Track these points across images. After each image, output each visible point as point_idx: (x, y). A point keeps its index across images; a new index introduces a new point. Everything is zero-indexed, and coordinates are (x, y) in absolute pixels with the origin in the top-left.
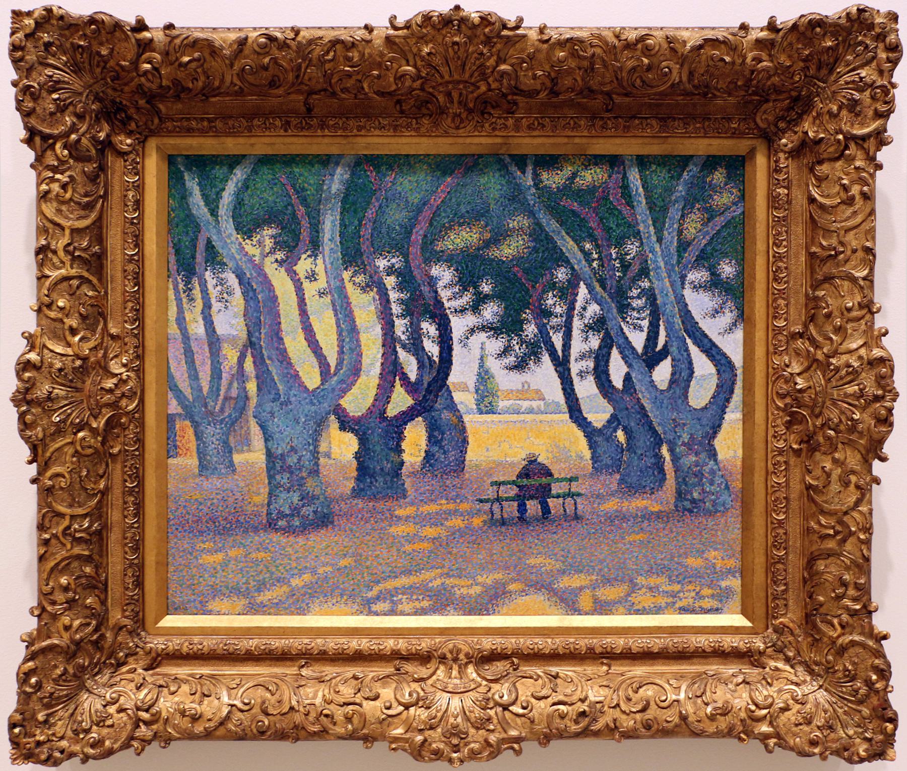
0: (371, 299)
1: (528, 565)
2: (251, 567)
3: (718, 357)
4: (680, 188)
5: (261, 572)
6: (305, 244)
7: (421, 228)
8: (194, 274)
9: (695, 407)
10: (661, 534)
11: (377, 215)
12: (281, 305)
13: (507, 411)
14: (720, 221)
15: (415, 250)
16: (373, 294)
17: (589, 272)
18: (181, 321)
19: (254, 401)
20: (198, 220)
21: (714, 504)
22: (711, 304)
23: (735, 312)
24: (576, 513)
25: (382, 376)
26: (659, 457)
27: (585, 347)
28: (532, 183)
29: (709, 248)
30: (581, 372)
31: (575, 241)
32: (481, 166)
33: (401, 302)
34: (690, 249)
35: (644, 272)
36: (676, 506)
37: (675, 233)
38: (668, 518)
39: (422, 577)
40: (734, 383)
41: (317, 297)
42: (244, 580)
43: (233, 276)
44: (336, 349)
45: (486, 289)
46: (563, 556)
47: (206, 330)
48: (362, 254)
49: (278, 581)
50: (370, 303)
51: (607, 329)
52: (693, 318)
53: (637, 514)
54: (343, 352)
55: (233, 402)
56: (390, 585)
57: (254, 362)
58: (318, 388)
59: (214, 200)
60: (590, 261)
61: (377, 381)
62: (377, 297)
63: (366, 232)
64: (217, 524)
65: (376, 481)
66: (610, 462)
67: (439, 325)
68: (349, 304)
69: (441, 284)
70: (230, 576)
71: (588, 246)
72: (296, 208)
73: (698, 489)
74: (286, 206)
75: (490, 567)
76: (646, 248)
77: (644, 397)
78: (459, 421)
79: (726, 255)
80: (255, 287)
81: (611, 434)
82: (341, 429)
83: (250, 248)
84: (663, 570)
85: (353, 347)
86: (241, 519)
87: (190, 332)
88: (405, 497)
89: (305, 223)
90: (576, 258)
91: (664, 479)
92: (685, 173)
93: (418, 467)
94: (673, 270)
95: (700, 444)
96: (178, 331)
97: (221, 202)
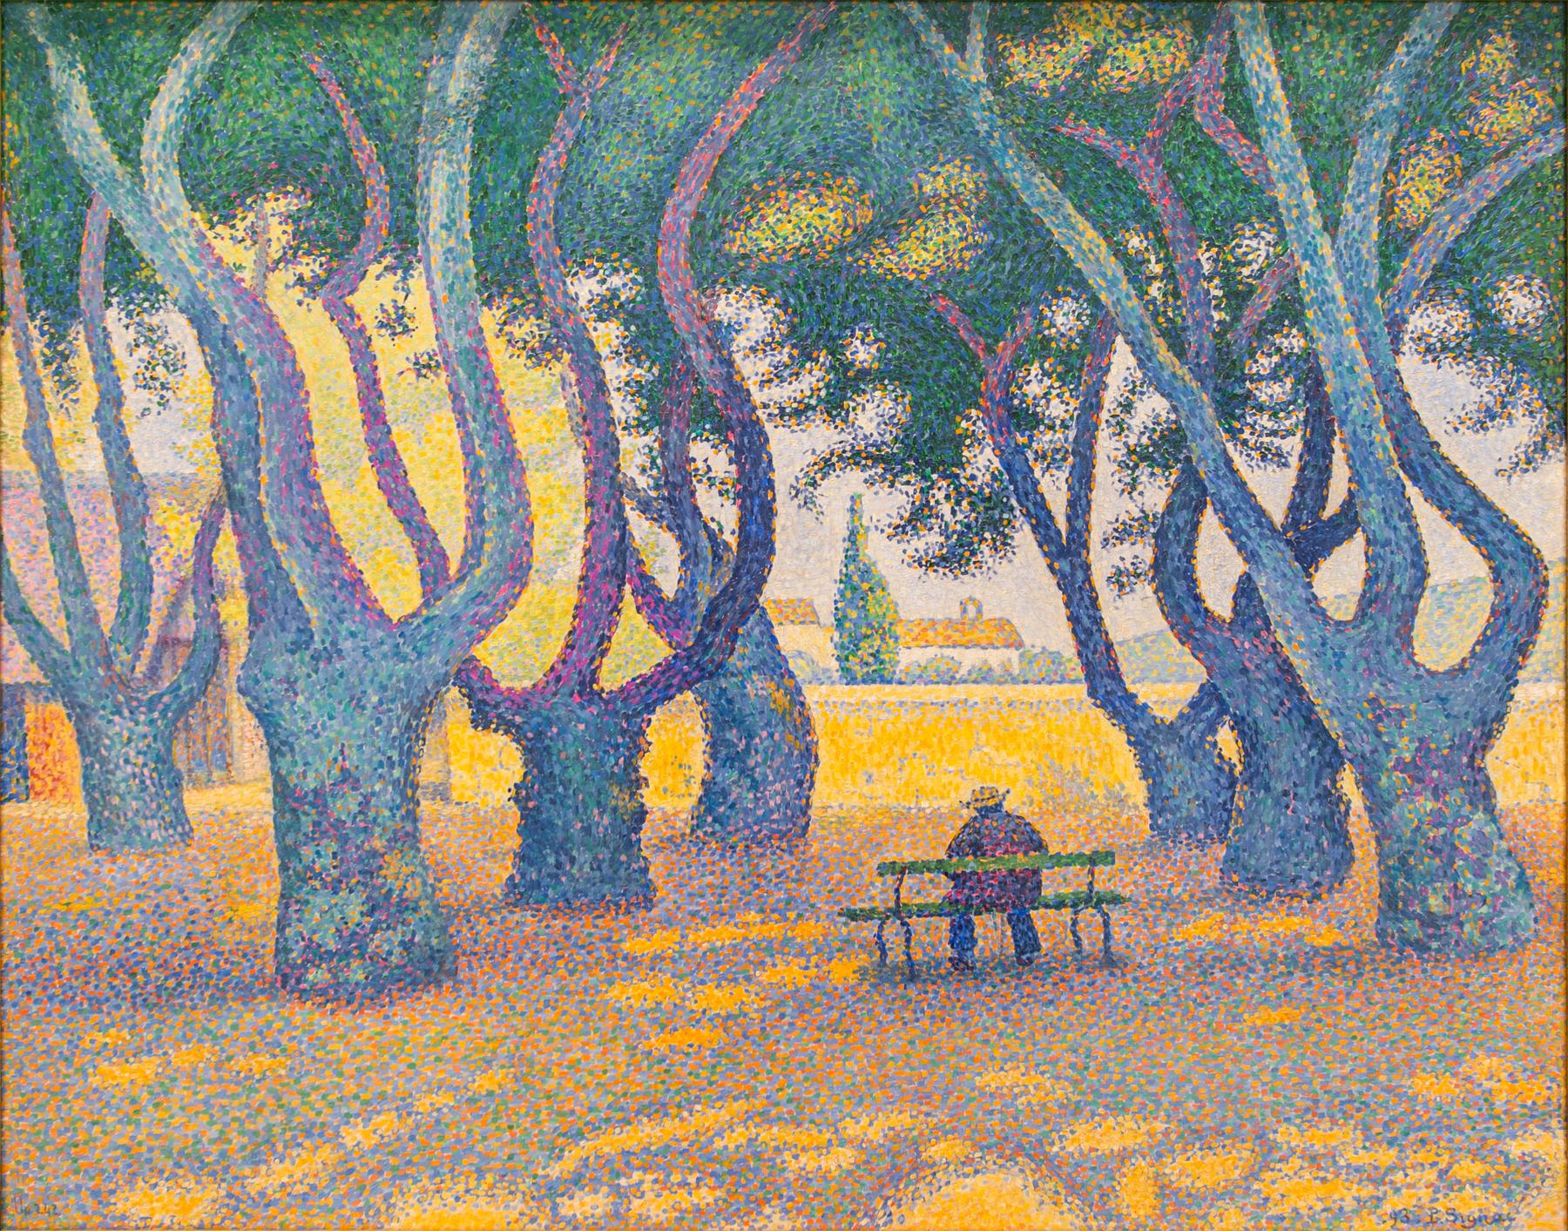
0: (555, 380)
1: (981, 1090)
2: (234, 1096)
3: (1496, 535)
4: (1388, 89)
5: (260, 1110)
6: (377, 238)
7: (689, 197)
8: (75, 315)
9: (1434, 668)
10: (1342, 1009)
11: (570, 162)
12: (312, 398)
13: (921, 677)
14: (1497, 175)
15: (672, 254)
16: (561, 367)
17: (1141, 311)
18: (38, 438)
19: (240, 649)
20: (84, 173)
21: (1487, 926)
22: (1474, 394)
23: (1543, 417)
24: (1107, 950)
25: (586, 583)
26: (1332, 800)
27: (1128, 508)
28: (983, 77)
29: (1468, 246)
30: (1119, 572)
31: (1102, 229)
32: (846, 32)
33: (636, 389)
34: (1415, 249)
35: (1289, 311)
36: (1381, 934)
37: (1373, 208)
38: (1359, 964)
39: (696, 1122)
40: (1539, 604)
41: (411, 376)
42: (214, 1132)
43: (182, 320)
44: (464, 512)
45: (861, 356)
46: (1073, 1066)
47: (109, 464)
48: (530, 264)
49: (308, 1134)
50: (554, 394)
51: (1188, 459)
52: (1425, 431)
53: (1274, 955)
54: (481, 522)
55: (182, 653)
56: (610, 1143)
57: (241, 548)
58: (414, 615)
59: (128, 120)
60: (1139, 281)
61: (574, 597)
62: (573, 377)
63: (543, 205)
64: (140, 978)
65: (573, 861)
66: (1198, 813)
67: (739, 450)
68: (496, 394)
69: (742, 341)
70: (176, 1121)
71: (1135, 242)
72: (352, 142)
73: (1444, 887)
74: (325, 137)
75: (877, 1093)
76: (1294, 246)
77: (1289, 639)
78: (792, 702)
79: (1516, 264)
80: (241, 349)
81: (1202, 738)
82: (475, 723)
83: (230, 248)
84: (1347, 1107)
85: (510, 506)
86: (207, 964)
87: (65, 468)
88: (648, 904)
89: (377, 182)
90: (1104, 275)
91: (1346, 860)
92: (1401, 49)
93: (682, 824)
94: (1370, 306)
95: (1447, 765)
96: (31, 466)
97: (149, 125)
